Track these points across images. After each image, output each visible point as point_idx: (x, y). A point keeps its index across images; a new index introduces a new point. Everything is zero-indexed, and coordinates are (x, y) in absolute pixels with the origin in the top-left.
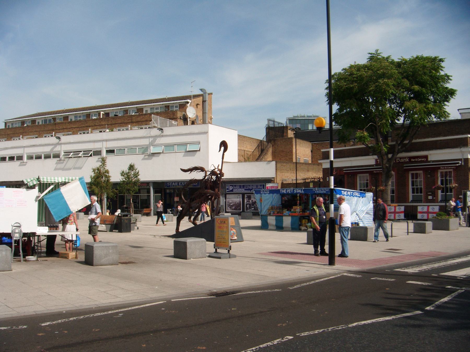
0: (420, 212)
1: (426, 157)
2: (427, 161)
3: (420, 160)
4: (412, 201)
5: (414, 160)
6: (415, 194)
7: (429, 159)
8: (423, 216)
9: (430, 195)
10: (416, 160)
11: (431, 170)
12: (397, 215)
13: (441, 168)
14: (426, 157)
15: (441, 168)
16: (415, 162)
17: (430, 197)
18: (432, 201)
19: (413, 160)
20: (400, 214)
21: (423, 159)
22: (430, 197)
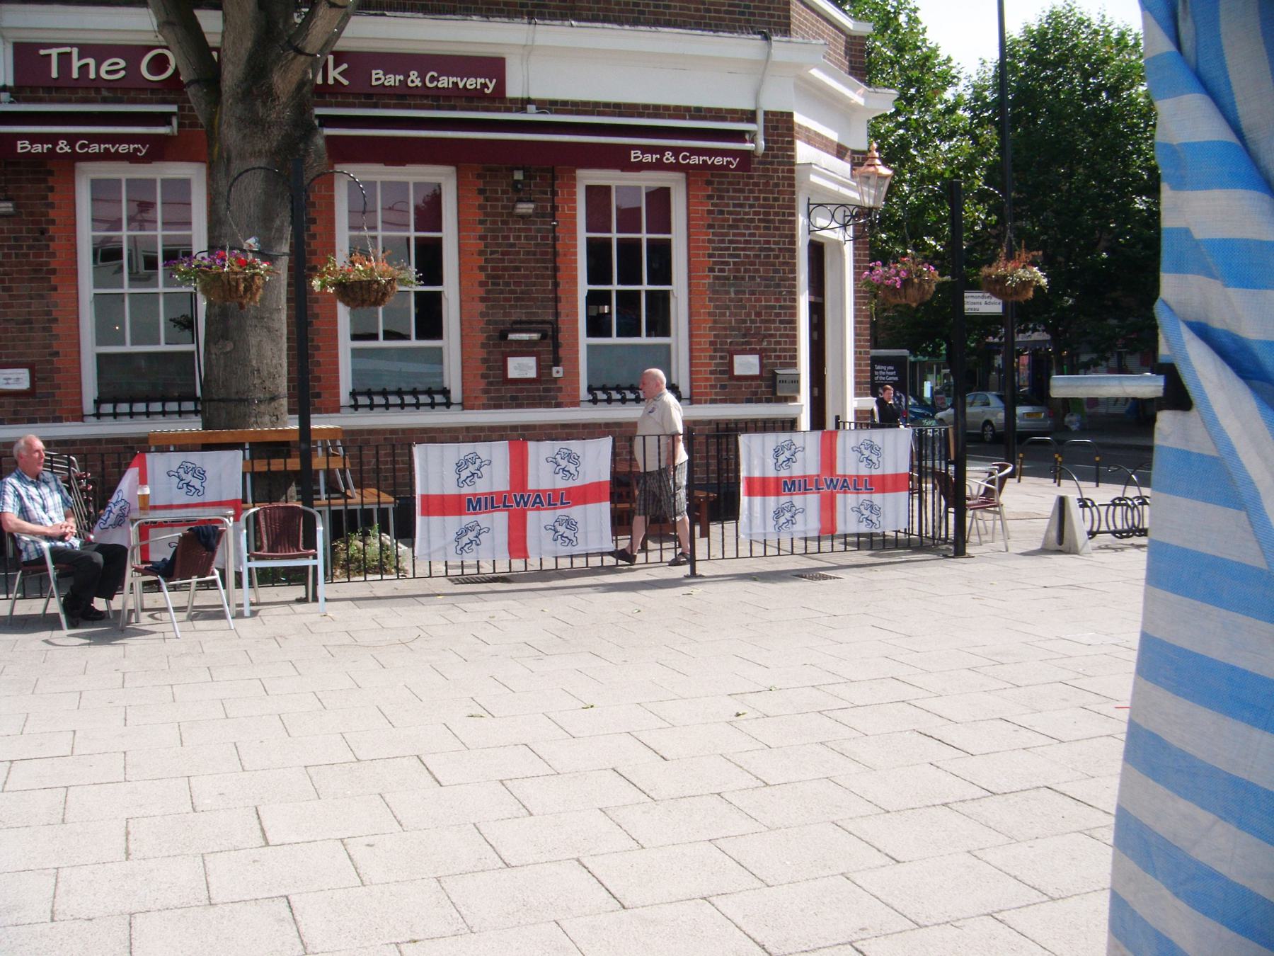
0: (763, 487)
1: (494, 67)
2: (498, 98)
3: (445, 82)
4: (366, 396)
5: (392, 80)
6: (644, 340)
7: (514, 90)
8: (564, 532)
9: (523, 349)
10: (414, 79)
11: (524, 162)
12: (847, 503)
13: (635, 155)
14: (494, 67)
15: (635, 155)
16: (402, 96)
17: (746, 365)
18: (542, 391)
19: (379, 77)
20: (576, 512)
21: (471, 83)
22: (522, 367)
